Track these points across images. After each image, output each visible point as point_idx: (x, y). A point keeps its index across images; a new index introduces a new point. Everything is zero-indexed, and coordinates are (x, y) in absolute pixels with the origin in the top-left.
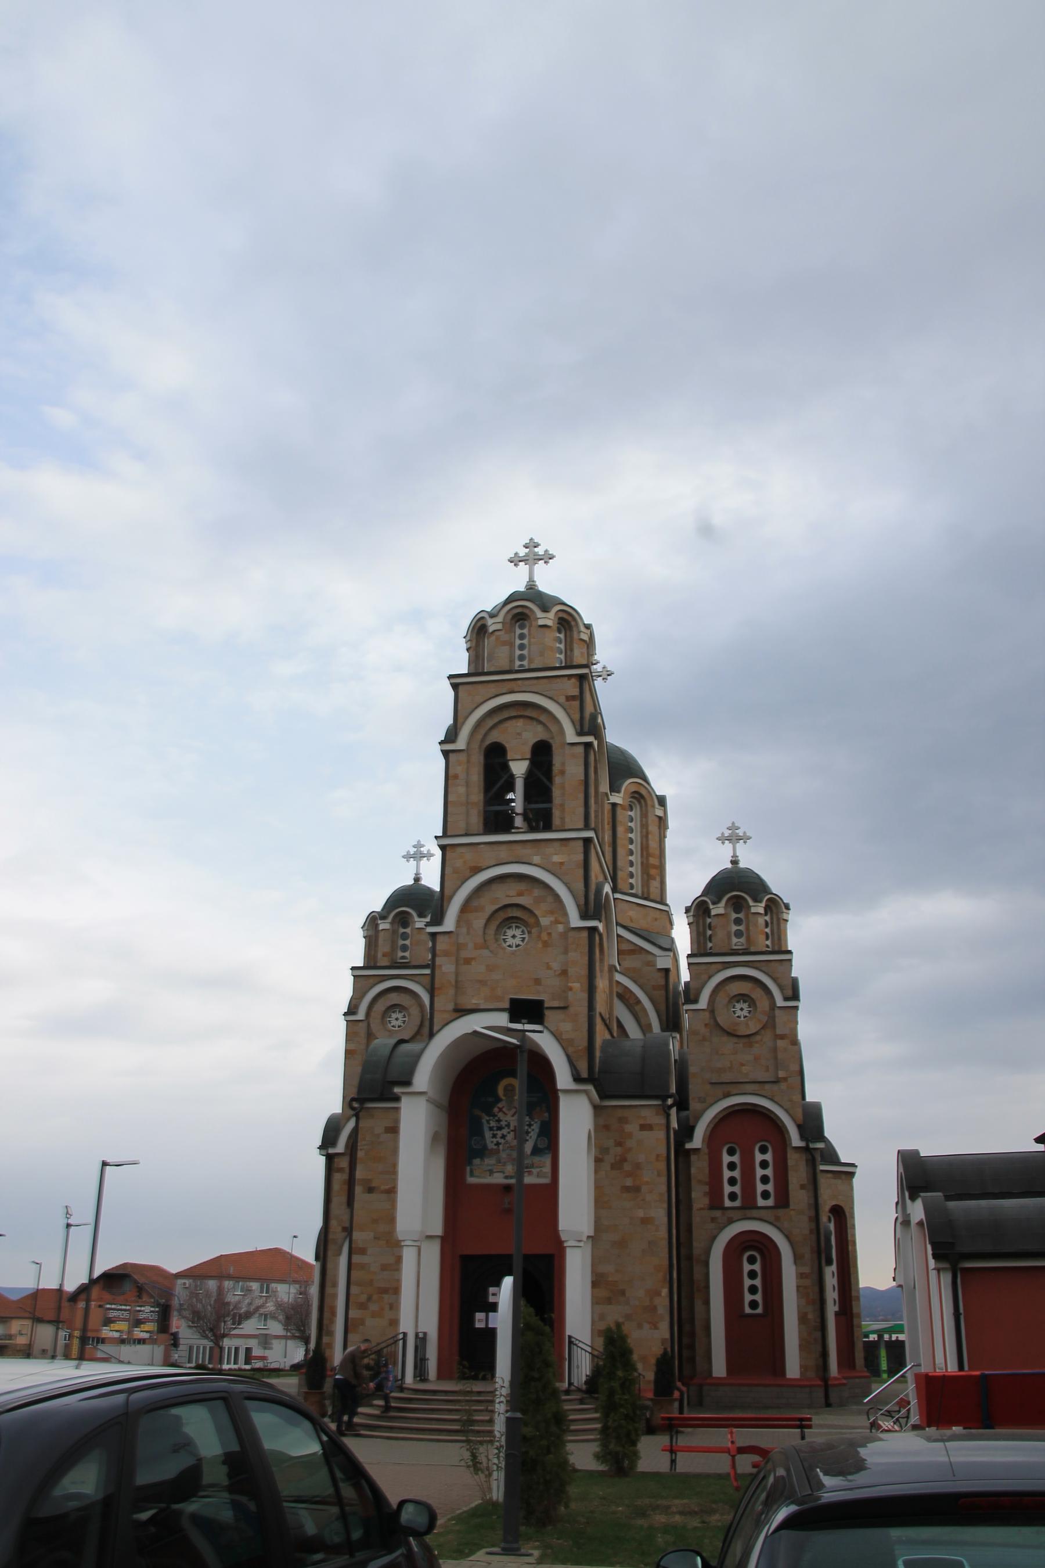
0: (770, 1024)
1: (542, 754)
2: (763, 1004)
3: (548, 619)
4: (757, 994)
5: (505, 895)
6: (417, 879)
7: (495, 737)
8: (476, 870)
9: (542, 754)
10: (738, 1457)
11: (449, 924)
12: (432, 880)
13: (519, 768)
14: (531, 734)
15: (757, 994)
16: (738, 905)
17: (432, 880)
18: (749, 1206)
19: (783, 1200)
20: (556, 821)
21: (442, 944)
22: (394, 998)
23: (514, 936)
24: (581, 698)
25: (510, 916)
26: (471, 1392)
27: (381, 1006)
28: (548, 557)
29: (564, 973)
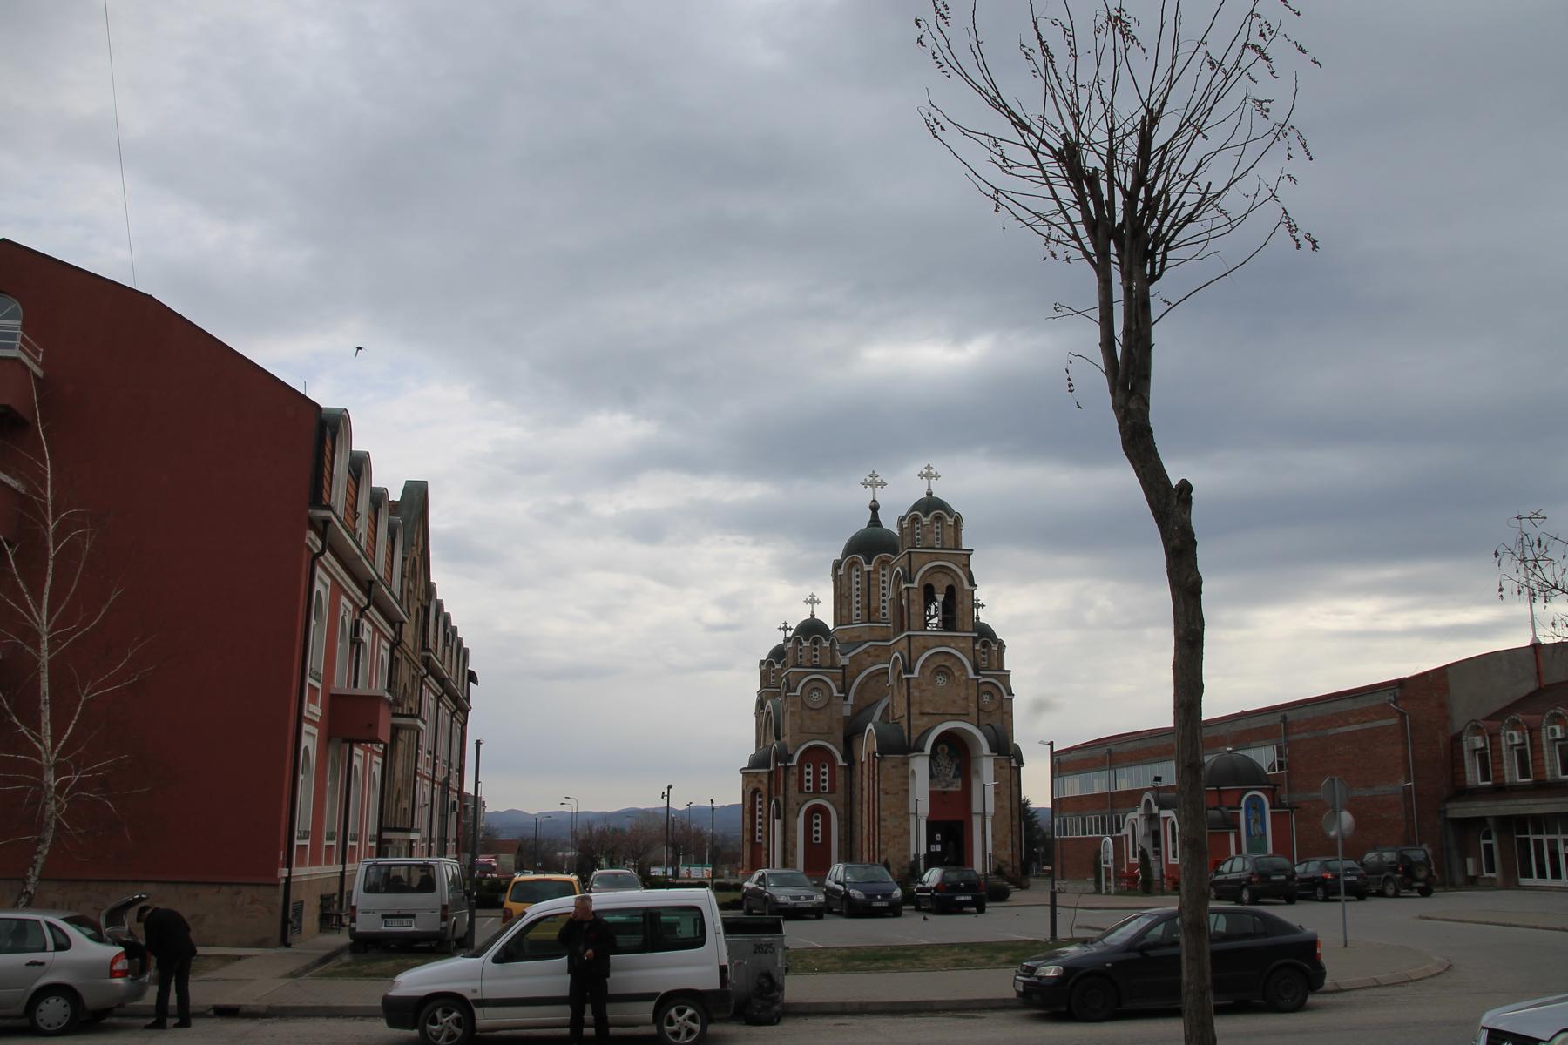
0: (1000, 706)
1: (951, 592)
2: (997, 696)
3: (951, 522)
4: (994, 691)
5: (940, 661)
6: (929, 494)
7: (929, 581)
8: (927, 648)
9: (951, 592)
10: (1044, 934)
11: (916, 674)
12: (826, 614)
13: (940, 597)
14: (947, 581)
15: (994, 691)
16: (984, 645)
17: (826, 614)
18: (817, 792)
19: (833, 790)
20: (959, 624)
21: (912, 683)
22: (815, 684)
23: (941, 680)
24: (969, 565)
25: (941, 670)
26: (1108, 878)
27: (808, 689)
28: (937, 476)
29: (966, 698)
